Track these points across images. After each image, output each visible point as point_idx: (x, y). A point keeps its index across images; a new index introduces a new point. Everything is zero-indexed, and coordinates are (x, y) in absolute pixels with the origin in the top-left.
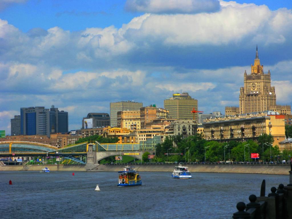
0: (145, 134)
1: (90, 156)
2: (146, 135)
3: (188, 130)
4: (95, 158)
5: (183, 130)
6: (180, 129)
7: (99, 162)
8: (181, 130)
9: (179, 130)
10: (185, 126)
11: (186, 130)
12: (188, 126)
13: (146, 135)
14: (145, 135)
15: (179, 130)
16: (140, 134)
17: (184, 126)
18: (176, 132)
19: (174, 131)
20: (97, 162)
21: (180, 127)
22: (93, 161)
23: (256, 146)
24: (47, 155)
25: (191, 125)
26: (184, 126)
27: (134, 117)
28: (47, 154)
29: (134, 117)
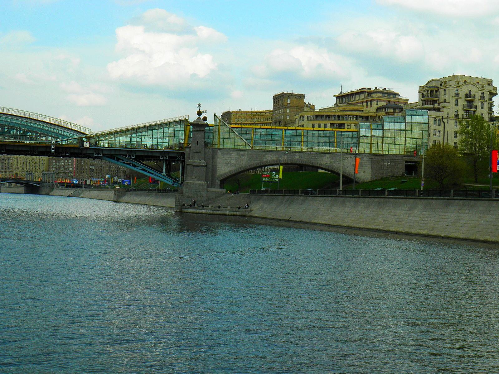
0: (328, 122)
1: (196, 161)
2: (331, 124)
3: (478, 103)
4: (213, 165)
5: (465, 103)
6: (459, 100)
7: (224, 182)
8: (462, 102)
9: (457, 105)
10: (472, 93)
11: (474, 104)
12: (480, 94)
13: (331, 124)
14: (329, 125)
15: (457, 105)
16: (313, 122)
17: (470, 91)
18: (448, 108)
19: (442, 105)
20: (218, 182)
21: (460, 95)
22: (206, 181)
23: (47, 188)
24: (53, 151)
25: (487, 90)
26: (470, 91)
27: (262, 119)
28: (53, 147)
29: (262, 119)
